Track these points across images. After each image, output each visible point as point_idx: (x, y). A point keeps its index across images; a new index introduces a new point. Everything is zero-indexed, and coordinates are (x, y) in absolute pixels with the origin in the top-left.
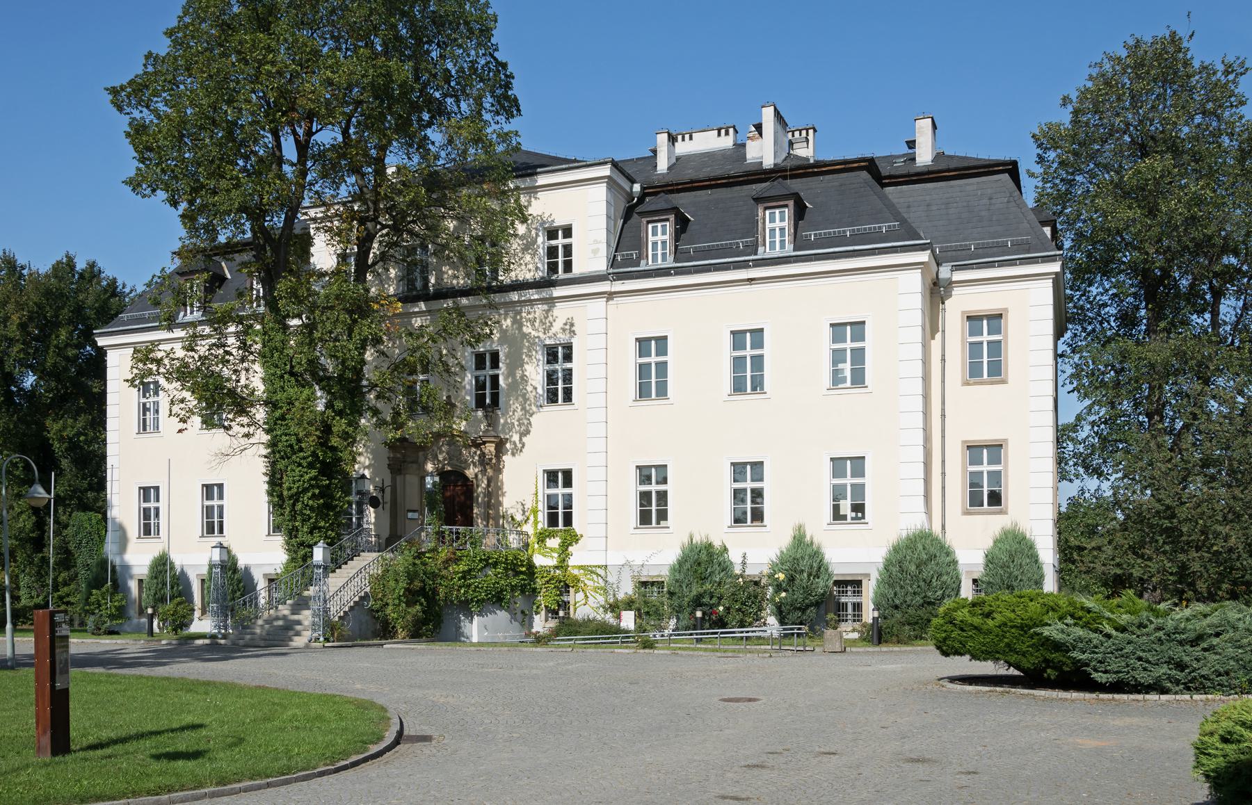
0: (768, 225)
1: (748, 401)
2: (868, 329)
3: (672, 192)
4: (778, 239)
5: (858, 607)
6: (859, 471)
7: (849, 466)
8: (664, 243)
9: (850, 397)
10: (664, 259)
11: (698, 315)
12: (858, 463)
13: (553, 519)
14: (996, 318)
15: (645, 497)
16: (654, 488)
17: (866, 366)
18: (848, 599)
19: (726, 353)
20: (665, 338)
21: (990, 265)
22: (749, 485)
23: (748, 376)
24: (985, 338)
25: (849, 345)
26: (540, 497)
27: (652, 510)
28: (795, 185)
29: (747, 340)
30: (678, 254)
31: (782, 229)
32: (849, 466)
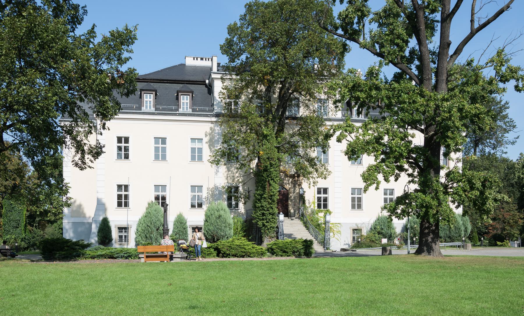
0: (182, 101)
3: (187, 84)
4: (148, 105)
8: (187, 103)
9: (160, 164)
12: (126, 187)
13: (319, 206)
15: (119, 197)
16: (123, 193)
17: (190, 154)
19: (153, 145)
22: (356, 196)
23: (160, 154)
25: (160, 146)
26: (316, 198)
28: (155, 86)
30: (155, 106)
31: (187, 103)
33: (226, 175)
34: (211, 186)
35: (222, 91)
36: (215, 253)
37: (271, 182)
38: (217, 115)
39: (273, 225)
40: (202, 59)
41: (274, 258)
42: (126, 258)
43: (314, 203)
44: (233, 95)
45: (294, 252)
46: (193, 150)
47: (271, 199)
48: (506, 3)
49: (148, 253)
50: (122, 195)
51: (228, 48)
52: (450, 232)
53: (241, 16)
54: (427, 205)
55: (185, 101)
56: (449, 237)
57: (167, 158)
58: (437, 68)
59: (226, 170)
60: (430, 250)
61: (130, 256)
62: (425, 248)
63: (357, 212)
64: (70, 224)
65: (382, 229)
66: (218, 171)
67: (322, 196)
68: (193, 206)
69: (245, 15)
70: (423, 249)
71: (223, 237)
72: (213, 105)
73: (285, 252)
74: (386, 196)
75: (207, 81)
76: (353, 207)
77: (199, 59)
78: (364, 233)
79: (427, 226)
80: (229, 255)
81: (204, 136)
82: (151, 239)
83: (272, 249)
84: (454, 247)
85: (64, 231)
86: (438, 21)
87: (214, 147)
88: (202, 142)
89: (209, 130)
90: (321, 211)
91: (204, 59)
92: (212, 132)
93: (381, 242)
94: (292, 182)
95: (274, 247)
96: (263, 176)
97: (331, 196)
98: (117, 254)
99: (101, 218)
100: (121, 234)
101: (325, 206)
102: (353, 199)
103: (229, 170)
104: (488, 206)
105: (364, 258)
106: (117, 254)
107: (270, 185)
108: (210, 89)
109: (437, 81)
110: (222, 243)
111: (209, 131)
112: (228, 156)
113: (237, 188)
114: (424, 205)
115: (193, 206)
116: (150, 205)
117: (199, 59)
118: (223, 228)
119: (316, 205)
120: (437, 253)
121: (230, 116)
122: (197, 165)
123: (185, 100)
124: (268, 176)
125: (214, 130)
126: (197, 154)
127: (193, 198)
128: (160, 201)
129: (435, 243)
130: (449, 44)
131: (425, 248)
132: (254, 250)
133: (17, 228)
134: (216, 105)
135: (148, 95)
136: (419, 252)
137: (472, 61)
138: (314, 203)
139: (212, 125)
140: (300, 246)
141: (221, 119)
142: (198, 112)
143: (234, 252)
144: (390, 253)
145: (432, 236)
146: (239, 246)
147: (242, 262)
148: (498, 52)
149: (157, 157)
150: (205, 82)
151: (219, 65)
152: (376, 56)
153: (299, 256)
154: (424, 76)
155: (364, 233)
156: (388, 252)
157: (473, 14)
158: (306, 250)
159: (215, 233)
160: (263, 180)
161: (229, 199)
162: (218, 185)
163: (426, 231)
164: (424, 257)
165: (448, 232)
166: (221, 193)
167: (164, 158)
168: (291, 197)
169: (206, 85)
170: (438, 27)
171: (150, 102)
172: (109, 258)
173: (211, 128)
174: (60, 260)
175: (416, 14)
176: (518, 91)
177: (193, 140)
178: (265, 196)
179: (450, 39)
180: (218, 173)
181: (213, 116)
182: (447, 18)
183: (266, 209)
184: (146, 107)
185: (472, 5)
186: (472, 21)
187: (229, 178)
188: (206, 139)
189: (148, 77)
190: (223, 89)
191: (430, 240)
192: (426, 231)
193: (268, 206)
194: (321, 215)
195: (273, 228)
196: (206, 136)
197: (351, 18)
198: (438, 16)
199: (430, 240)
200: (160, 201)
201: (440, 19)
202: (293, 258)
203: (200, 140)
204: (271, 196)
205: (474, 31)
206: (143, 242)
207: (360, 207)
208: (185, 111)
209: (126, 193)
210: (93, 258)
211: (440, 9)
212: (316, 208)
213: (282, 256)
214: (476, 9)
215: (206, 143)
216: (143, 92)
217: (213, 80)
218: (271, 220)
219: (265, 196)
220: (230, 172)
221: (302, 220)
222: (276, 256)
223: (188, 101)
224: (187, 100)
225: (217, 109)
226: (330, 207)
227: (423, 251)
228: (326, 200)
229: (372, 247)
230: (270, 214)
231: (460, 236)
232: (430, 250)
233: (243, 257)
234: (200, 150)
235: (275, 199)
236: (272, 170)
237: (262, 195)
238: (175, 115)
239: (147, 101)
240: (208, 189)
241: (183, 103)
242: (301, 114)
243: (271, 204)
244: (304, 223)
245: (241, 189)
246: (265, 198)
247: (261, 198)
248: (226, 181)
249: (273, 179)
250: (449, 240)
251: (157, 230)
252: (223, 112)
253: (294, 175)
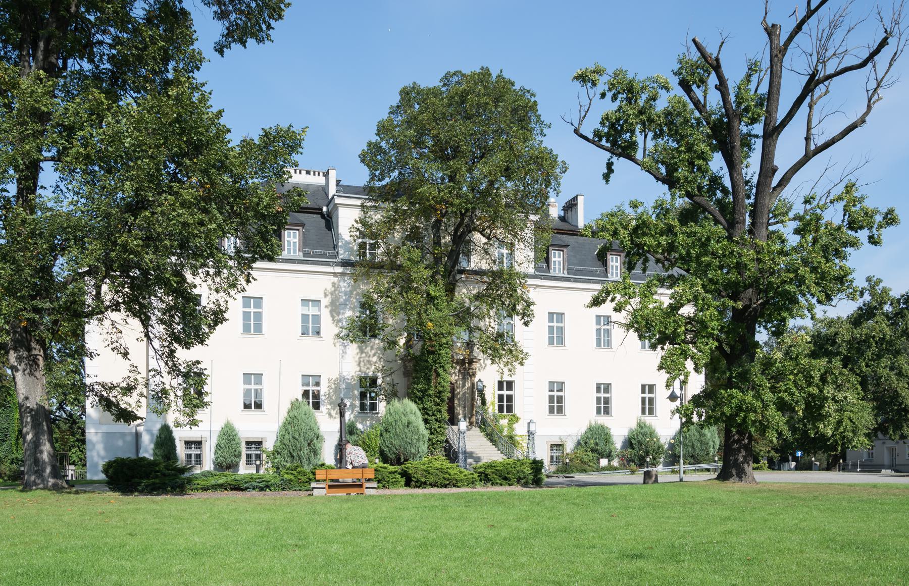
0: (287, 239)
9: (556, 350)
13: (501, 409)
17: (242, 322)
22: (556, 394)
25: (252, 310)
31: (294, 242)
33: (357, 359)
34: (335, 376)
35: (356, 225)
36: (403, 481)
37: (440, 371)
38: (345, 263)
39: (440, 438)
40: (308, 173)
41: (491, 489)
42: (262, 489)
43: (493, 404)
44: (366, 230)
45: (519, 480)
46: (305, 318)
47: (438, 397)
48: (860, 115)
49: (332, 480)
51: (372, 157)
52: (694, 449)
53: (392, 107)
54: (747, 407)
55: (292, 239)
56: (692, 456)
57: (265, 329)
58: (754, 205)
59: (358, 350)
60: (741, 474)
61: (267, 487)
62: (734, 471)
63: (556, 418)
64: (100, 435)
65: (597, 444)
66: (346, 353)
67: (505, 393)
68: (247, 406)
69: (398, 106)
70: (731, 472)
71: (414, 455)
72: (335, 247)
73: (505, 479)
74: (552, 394)
75: (325, 209)
76: (551, 410)
77: (304, 172)
78: (569, 448)
79: (736, 438)
80: (425, 483)
81: (323, 295)
82: (300, 458)
83: (486, 475)
84: (702, 470)
85: (88, 446)
86: (757, 136)
87: (338, 314)
88: (319, 306)
89: (330, 286)
90: (505, 417)
91: (312, 173)
92: (335, 291)
93: (599, 463)
94: (460, 371)
95: (489, 471)
96: (427, 361)
97: (518, 393)
98: (246, 483)
99: (158, 426)
100: (189, 452)
101: (510, 409)
102: (551, 398)
103: (362, 351)
104: (827, 409)
105: (612, 487)
106: (246, 483)
107: (438, 375)
108: (329, 221)
109: (753, 224)
110: (412, 466)
111: (330, 288)
112: (366, 329)
113: (374, 381)
114: (744, 407)
115: (247, 406)
116: (295, 405)
117: (304, 172)
118: (415, 441)
119: (496, 407)
120: (750, 478)
121: (362, 266)
122: (311, 341)
124: (435, 362)
125: (339, 286)
126: (252, 322)
127: (247, 393)
128: (311, 400)
129: (748, 463)
130: (775, 170)
131: (734, 471)
132: (462, 476)
133: (4, 441)
134: (341, 247)
136: (724, 476)
137: (813, 198)
138: (493, 404)
139: (335, 279)
140: (527, 470)
141: (349, 270)
142: (312, 257)
143: (432, 479)
144: (656, 481)
145: (743, 453)
146: (440, 470)
148: (846, 187)
150: (321, 209)
151: (338, 182)
152: (660, 182)
153: (526, 485)
154: (737, 217)
155: (569, 448)
156: (653, 478)
157: (809, 129)
158: (535, 476)
159: (402, 449)
160: (427, 368)
161: (363, 395)
162: (345, 374)
163: (736, 446)
164: (733, 485)
165: (690, 449)
166: (349, 387)
167: (258, 329)
168: (459, 393)
170: (758, 144)
171: (294, 242)
172: (232, 489)
173: (334, 284)
174: (141, 492)
175: (729, 123)
176: (872, 243)
177: (305, 301)
178: (430, 392)
179: (775, 163)
180: (346, 356)
181: (337, 264)
182: (772, 133)
183: (430, 413)
185: (809, 116)
186: (807, 139)
187: (362, 364)
188: (325, 301)
190: (356, 221)
191: (741, 459)
192: (736, 446)
193: (435, 408)
194: (504, 422)
195: (441, 442)
196: (326, 295)
197: (632, 124)
198: (758, 129)
199: (741, 459)
200: (311, 400)
201: (761, 133)
202: (517, 489)
203: (317, 302)
204: (440, 392)
205: (811, 154)
206: (288, 465)
207: (560, 410)
208: (292, 256)
209: (509, 393)
210: (205, 489)
211: (763, 118)
212: (497, 411)
213: (501, 485)
214: (814, 123)
215: (326, 307)
217: (336, 207)
218: (438, 430)
219: (430, 392)
220: (364, 355)
221: (482, 430)
222: (493, 484)
223: (297, 240)
224: (295, 237)
225: (343, 254)
226: (518, 410)
227: (732, 476)
228: (510, 398)
229: (586, 471)
230: (436, 420)
231: (707, 454)
232: (741, 474)
233: (445, 486)
234: (316, 318)
235: (446, 398)
236: (442, 352)
237: (426, 390)
240: (329, 381)
241: (289, 242)
242: (473, 265)
243: (439, 404)
244: (487, 435)
245: (380, 381)
246: (429, 395)
247: (424, 396)
248: (358, 369)
249: (443, 367)
250: (692, 461)
251: (309, 444)
252: (353, 258)
253: (463, 360)
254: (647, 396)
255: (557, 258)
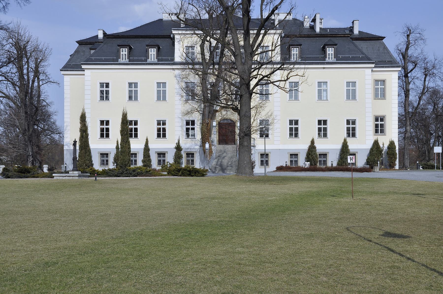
1: (105, 103)
2: (357, 84)
4: (124, 57)
5: (136, 161)
6: (164, 124)
7: (161, 123)
8: (297, 54)
10: (154, 59)
11: (310, 76)
14: (383, 81)
16: (322, 126)
17: (110, 95)
18: (133, 159)
20: (109, 83)
21: (383, 67)
24: (379, 87)
25: (133, 89)
27: (294, 133)
29: (161, 85)
30: (129, 58)
31: (332, 54)
32: (161, 123)
50: (104, 128)
57: (357, 98)
63: (294, 140)
76: (291, 135)
100: (160, 159)
123: (330, 51)
135: (124, 49)
147: (119, 180)
149: (159, 99)
169: (171, 38)
184: (329, 59)
189: (125, 35)
207: (296, 135)
216: (291, 47)
238: (323, 64)
239: (294, 54)
254: (294, 126)
255: (295, 51)
